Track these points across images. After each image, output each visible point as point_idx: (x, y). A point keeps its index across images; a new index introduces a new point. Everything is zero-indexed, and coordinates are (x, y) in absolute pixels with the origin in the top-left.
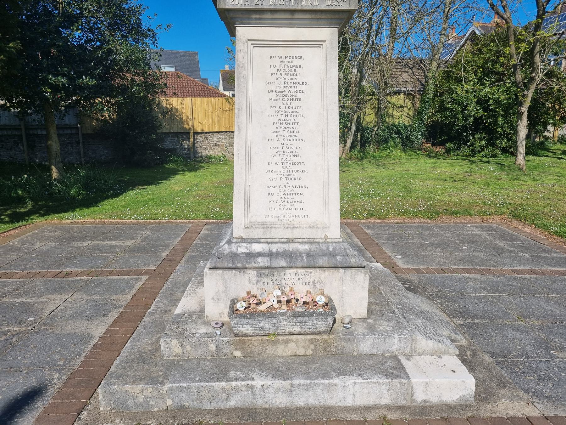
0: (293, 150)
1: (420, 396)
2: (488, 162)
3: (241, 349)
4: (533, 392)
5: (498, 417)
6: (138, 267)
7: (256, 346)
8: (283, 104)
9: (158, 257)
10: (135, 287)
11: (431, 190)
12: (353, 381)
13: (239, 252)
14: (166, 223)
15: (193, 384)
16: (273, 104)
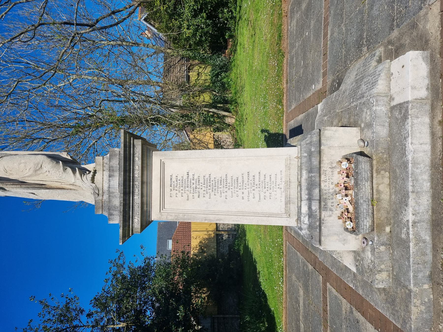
0: (233, 181)
1: (423, 93)
2: (240, 7)
3: (384, 226)
4: (421, 3)
5: (441, 34)
6: (320, 289)
7: (381, 215)
8: (201, 189)
9: (312, 272)
10: (336, 294)
11: (261, 55)
12: (410, 144)
13: (308, 223)
14: (286, 261)
15: (411, 268)
16: (201, 195)
